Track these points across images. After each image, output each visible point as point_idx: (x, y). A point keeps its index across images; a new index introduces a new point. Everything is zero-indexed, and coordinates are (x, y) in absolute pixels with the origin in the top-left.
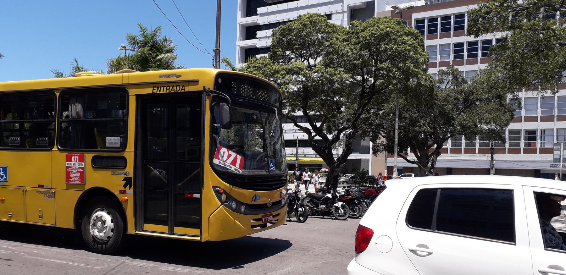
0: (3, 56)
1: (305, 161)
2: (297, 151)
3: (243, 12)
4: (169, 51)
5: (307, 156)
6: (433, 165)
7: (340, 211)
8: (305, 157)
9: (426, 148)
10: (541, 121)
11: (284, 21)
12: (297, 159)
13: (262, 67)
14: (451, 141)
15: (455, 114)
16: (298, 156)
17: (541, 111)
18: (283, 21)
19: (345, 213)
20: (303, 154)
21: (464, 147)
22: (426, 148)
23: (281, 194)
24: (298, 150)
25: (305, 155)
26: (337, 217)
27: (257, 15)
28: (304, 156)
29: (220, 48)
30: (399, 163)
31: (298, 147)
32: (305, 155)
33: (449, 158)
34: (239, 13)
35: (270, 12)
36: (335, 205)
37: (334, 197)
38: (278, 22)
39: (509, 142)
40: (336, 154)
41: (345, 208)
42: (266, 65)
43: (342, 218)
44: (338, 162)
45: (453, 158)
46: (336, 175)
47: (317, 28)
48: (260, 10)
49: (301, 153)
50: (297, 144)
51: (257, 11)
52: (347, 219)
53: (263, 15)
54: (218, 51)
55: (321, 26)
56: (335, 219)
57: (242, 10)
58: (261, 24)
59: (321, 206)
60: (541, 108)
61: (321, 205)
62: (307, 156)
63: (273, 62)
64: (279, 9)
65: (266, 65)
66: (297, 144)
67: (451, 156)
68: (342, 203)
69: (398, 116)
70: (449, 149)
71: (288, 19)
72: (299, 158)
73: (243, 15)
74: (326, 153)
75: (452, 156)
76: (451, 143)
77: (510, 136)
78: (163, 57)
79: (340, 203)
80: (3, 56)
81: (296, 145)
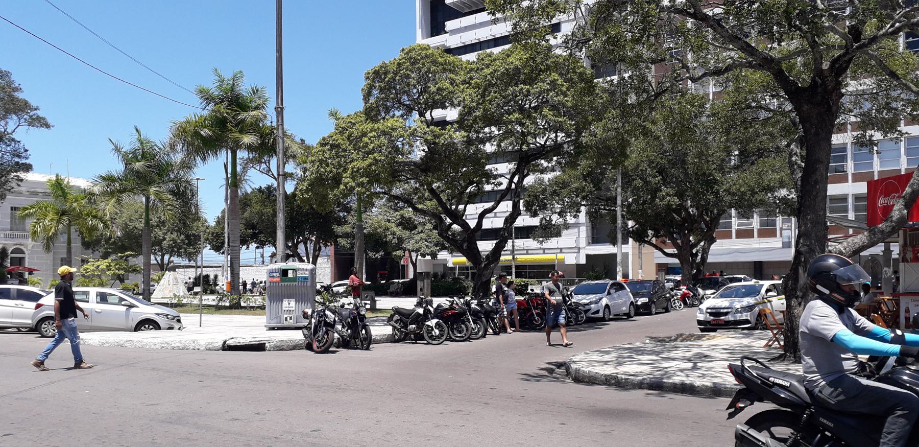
0: (53, 126)
1: (526, 260)
2: (513, 246)
3: (424, 32)
4: (257, 108)
5: (529, 252)
6: (704, 259)
7: (433, 332)
8: (527, 254)
9: (686, 232)
10: (854, 181)
11: (503, 35)
12: (513, 258)
13: (350, 127)
14: (760, 218)
15: (718, 176)
16: (515, 252)
17: (905, 160)
18: (485, 39)
19: (441, 335)
20: (524, 250)
21: (758, 228)
22: (686, 232)
23: (759, 318)
24: (515, 244)
25: (527, 250)
26: (430, 341)
27: (446, 33)
28: (525, 252)
29: (282, 104)
30: (740, 254)
31: (516, 238)
32: (527, 252)
33: (757, 246)
34: (419, 32)
35: (466, 27)
36: (427, 323)
37: (427, 311)
38: (493, 38)
39: (855, 215)
40: (575, 247)
41: (442, 327)
42: (354, 124)
43: (436, 342)
44: (486, 261)
45: (762, 246)
46: (485, 280)
47: (417, 66)
48: (450, 25)
49: (519, 248)
50: (514, 235)
51: (444, 26)
52: (445, 342)
53: (454, 32)
54: (280, 109)
55: (423, 64)
56: (426, 344)
57: (424, 27)
58: (452, 47)
59: (411, 326)
60: (907, 154)
61: (410, 325)
62: (529, 252)
63: (596, 87)
64: (463, 25)
65: (354, 124)
66: (514, 235)
67: (759, 242)
68: (438, 320)
69: (620, 185)
70: (755, 231)
71: (493, 36)
72: (518, 257)
73: (425, 34)
74: (465, 248)
75: (761, 241)
76: (758, 221)
77: (855, 205)
78: (245, 117)
79: (435, 321)
80: (53, 126)
81: (512, 236)
